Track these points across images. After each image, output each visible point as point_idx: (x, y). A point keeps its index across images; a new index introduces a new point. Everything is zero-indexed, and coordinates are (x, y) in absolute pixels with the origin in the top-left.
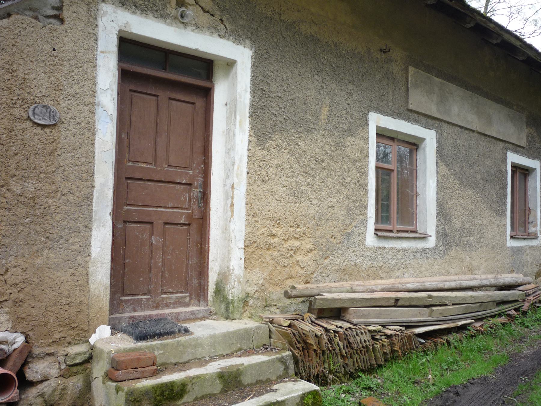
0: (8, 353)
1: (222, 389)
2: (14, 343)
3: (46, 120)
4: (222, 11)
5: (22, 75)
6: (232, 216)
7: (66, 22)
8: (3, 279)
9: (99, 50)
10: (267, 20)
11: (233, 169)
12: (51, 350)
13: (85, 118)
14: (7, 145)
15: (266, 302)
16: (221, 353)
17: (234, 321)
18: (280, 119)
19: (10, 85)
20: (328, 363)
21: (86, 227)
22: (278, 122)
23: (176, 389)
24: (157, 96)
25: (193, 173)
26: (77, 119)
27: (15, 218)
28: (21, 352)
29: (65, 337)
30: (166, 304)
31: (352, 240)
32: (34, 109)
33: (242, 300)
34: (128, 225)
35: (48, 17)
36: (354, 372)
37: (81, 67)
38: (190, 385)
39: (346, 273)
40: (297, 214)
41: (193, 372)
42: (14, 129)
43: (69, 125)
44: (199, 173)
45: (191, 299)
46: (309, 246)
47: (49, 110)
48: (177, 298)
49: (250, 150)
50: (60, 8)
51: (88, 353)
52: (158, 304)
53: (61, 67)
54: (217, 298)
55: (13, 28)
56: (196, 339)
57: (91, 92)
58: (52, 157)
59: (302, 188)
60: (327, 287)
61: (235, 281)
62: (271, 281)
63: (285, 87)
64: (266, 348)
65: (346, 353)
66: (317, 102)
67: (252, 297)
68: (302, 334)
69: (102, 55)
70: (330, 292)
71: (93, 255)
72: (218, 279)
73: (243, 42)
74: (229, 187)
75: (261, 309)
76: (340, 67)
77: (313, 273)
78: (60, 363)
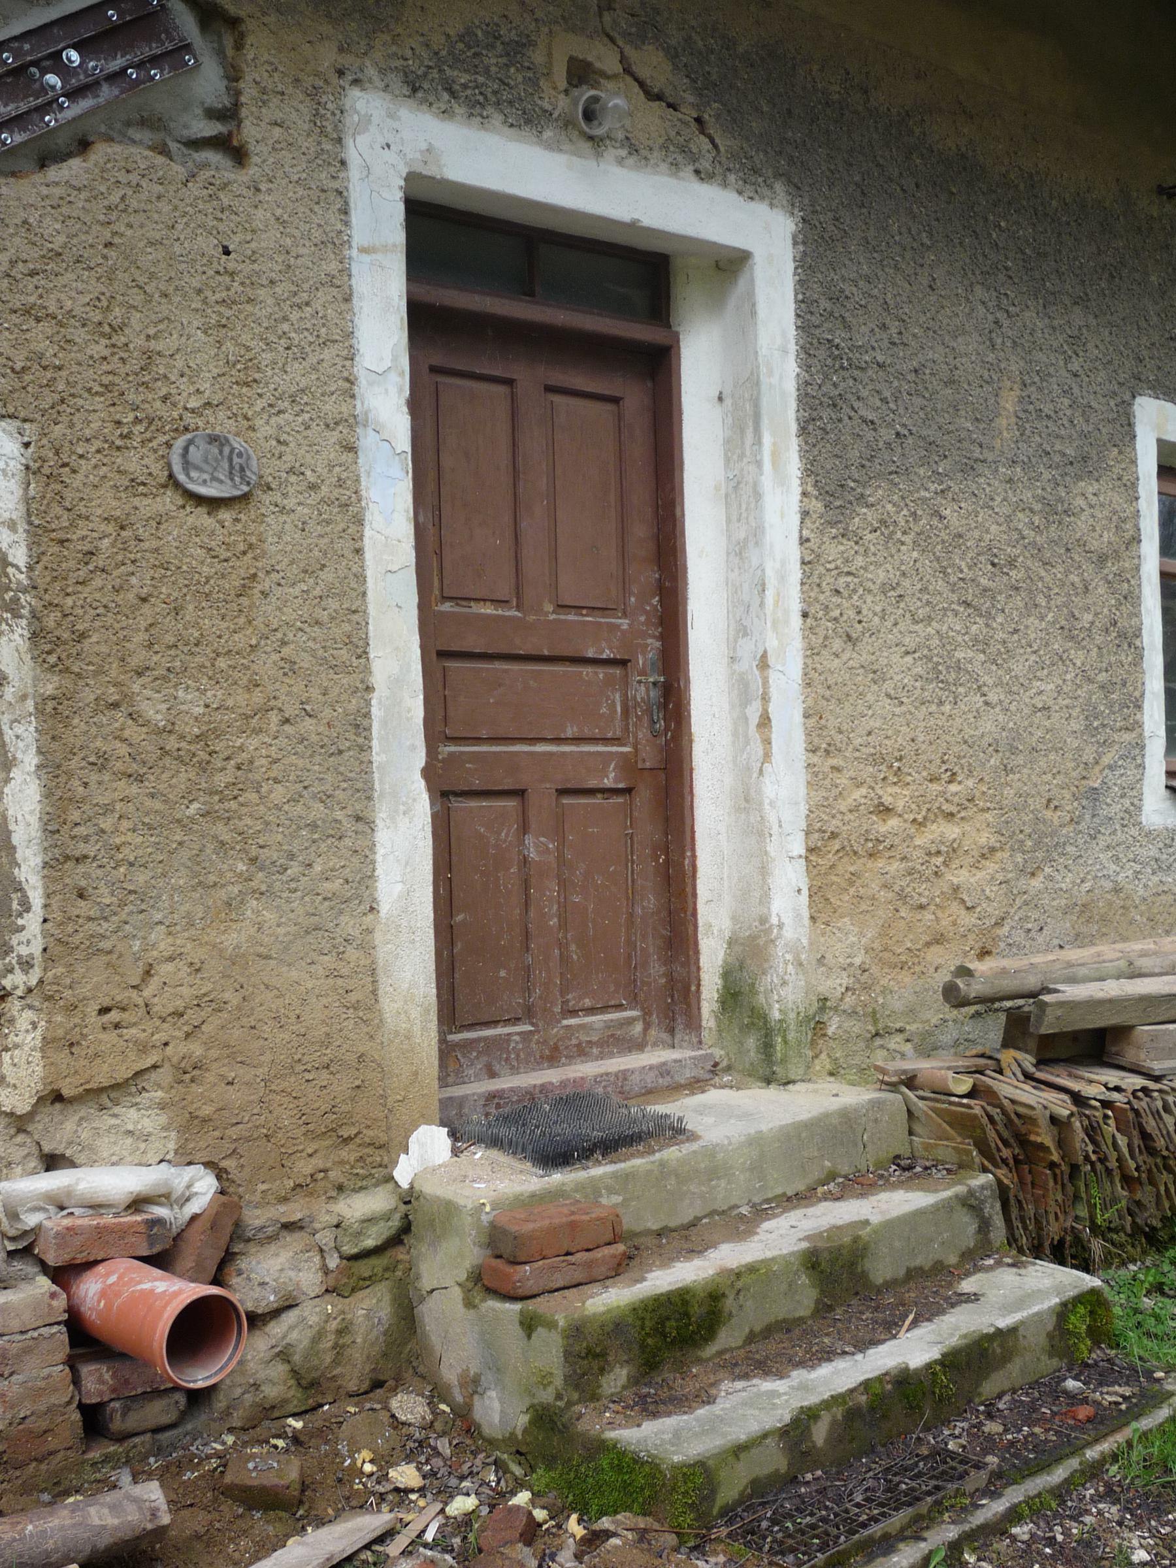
0: (175, 1231)
1: (818, 1302)
2: (188, 1200)
3: (221, 482)
4: (699, 92)
5: (140, 341)
6: (767, 756)
7: (255, 159)
8: (140, 1001)
9: (354, 244)
10: (828, 112)
11: (762, 605)
12: (294, 1211)
13: (331, 467)
14: (116, 573)
15: (875, 1022)
16: (779, 1191)
17: (790, 1086)
18: (887, 434)
19: (110, 377)
20: (1088, 1201)
21: (358, 819)
22: (881, 444)
23: (696, 1311)
24: (509, 382)
25: (630, 625)
26: (308, 473)
27: (158, 805)
28: (214, 1226)
29: (325, 1171)
30: (579, 1045)
31: (1104, 812)
32: (186, 449)
33: (808, 1019)
34: (456, 803)
35: (196, 144)
36: (1159, 1225)
37: (307, 304)
38: (731, 1297)
39: (1093, 917)
40: (948, 738)
41: (729, 1255)
42: (133, 519)
43: (285, 495)
44: (647, 622)
45: (647, 1026)
46: (986, 838)
47: (227, 450)
48: (608, 1025)
49: (808, 540)
50: (229, 114)
51: (398, 1216)
52: (556, 1048)
53: (249, 308)
54: (730, 1019)
55: (103, 189)
56: (711, 1152)
57: (340, 383)
58: (244, 601)
59: (959, 655)
60: (1058, 966)
61: (786, 963)
62: (886, 955)
63: (894, 331)
64: (906, 1168)
65: (1137, 1169)
66: (986, 376)
67: (835, 1009)
68: (1013, 1116)
69: (366, 258)
70: (1072, 980)
71: (384, 908)
72: (730, 959)
73: (765, 191)
74: (748, 664)
75: (862, 1045)
76: (1045, 255)
77: (999, 924)
78: (321, 1251)
